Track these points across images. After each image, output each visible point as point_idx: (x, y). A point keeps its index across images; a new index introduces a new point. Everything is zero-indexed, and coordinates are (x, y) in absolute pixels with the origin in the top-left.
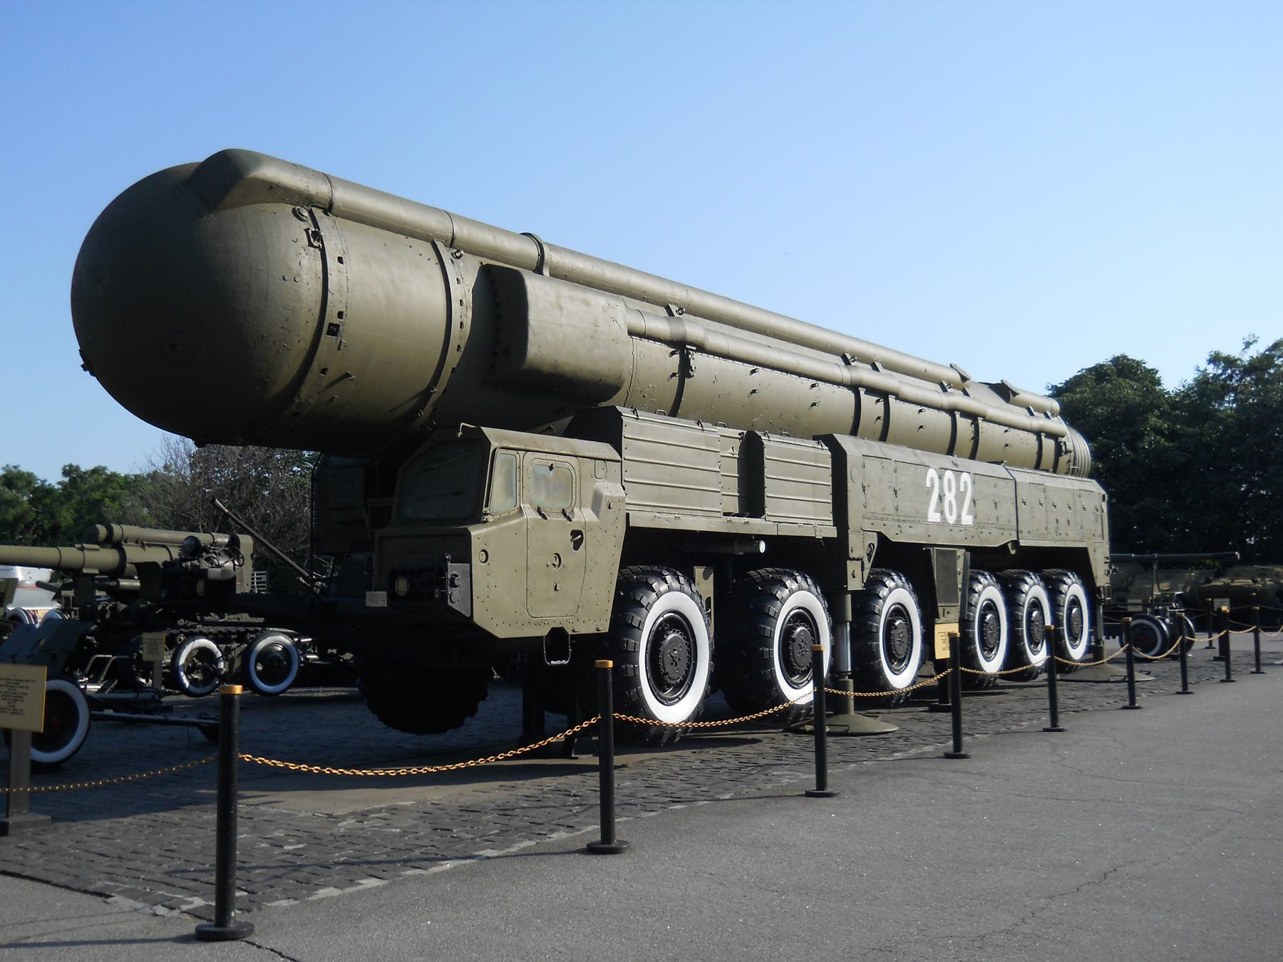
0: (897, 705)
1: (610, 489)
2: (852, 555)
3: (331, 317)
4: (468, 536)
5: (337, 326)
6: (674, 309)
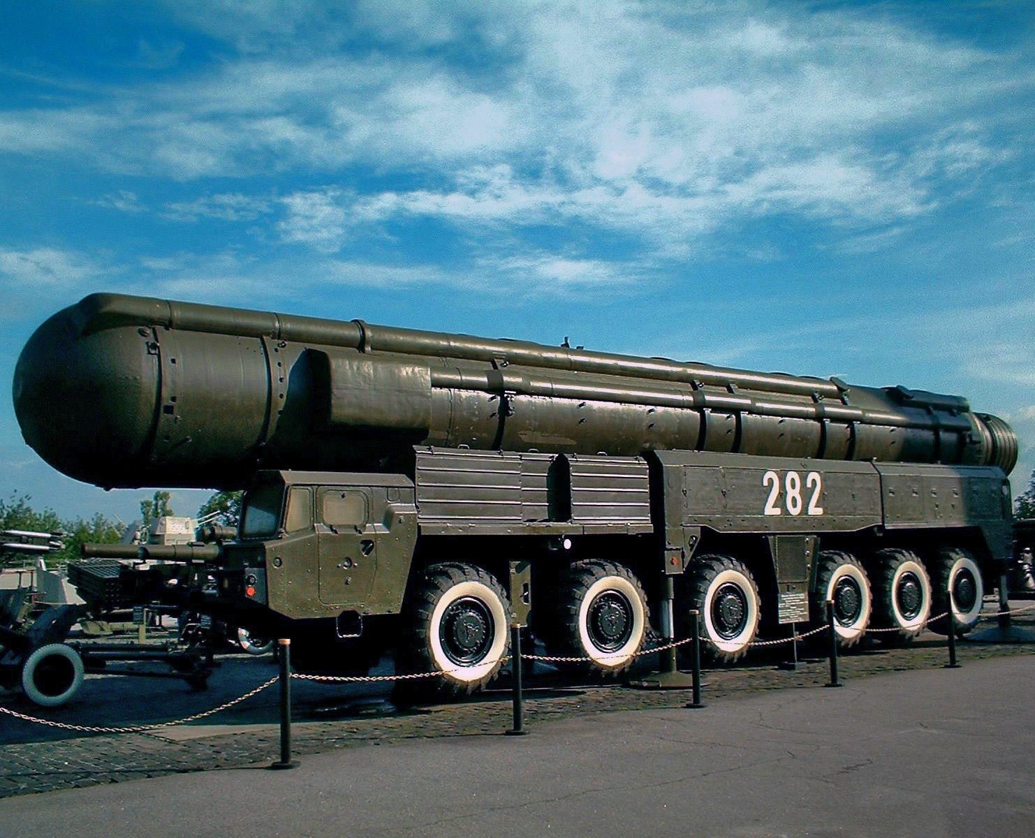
1: (402, 508)
2: (668, 547)
3: (166, 401)
4: (263, 547)
5: (172, 407)
6: (817, 395)
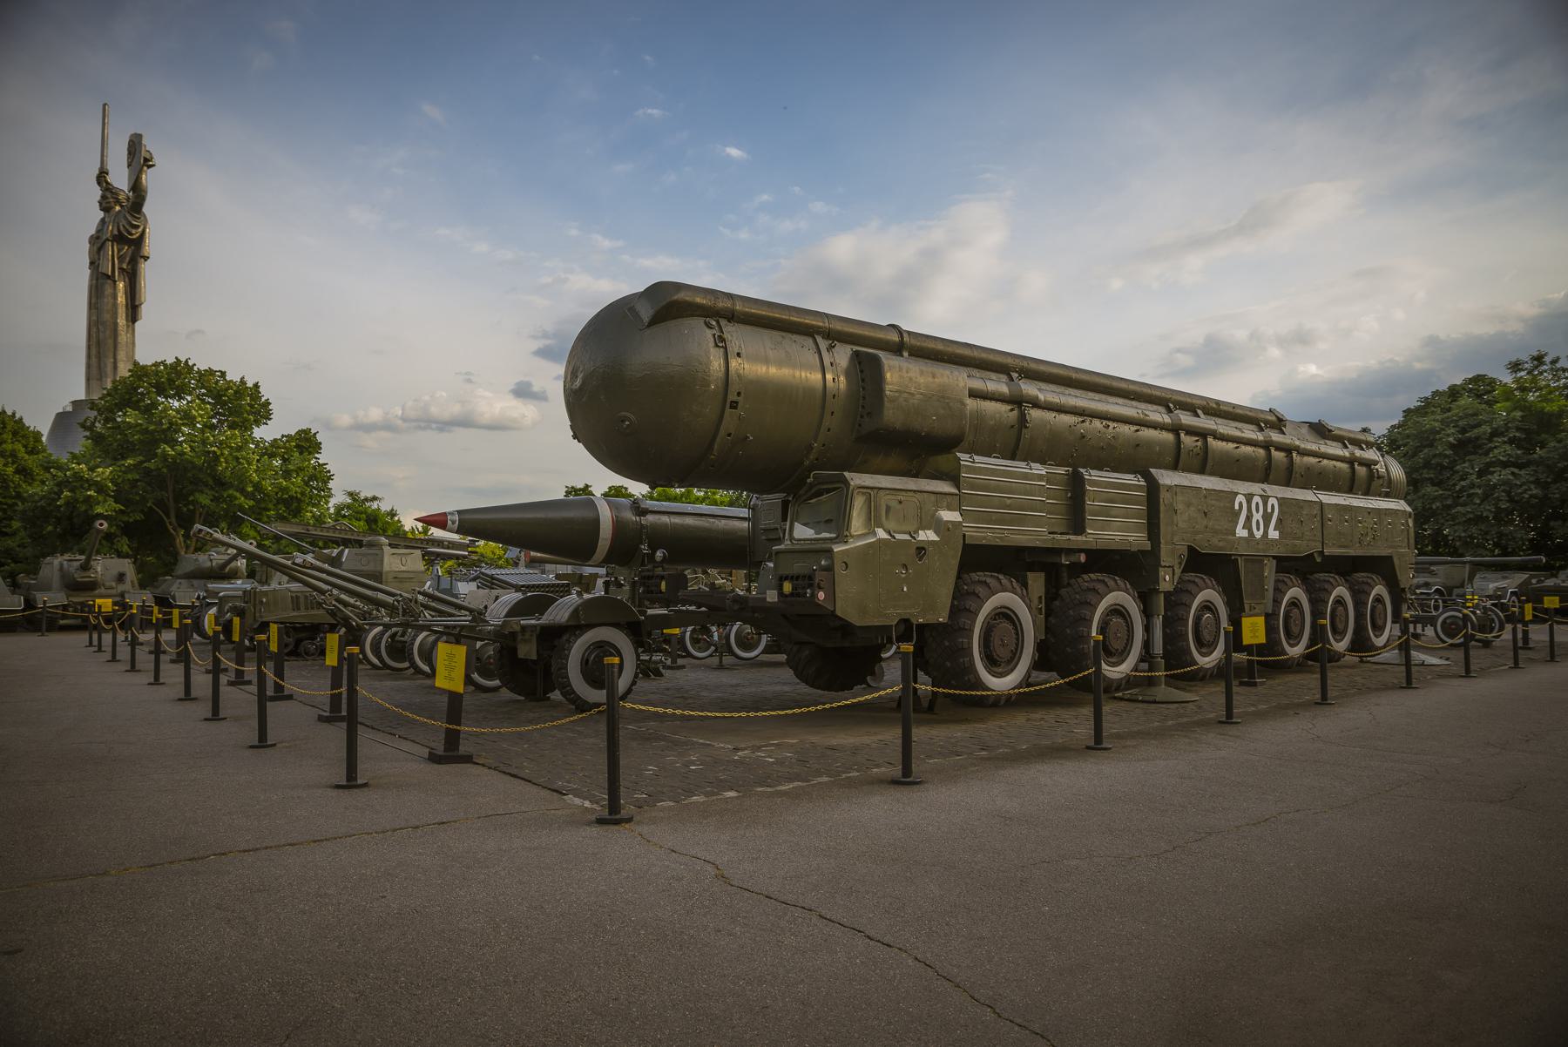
0: (1203, 679)
3: (732, 397)
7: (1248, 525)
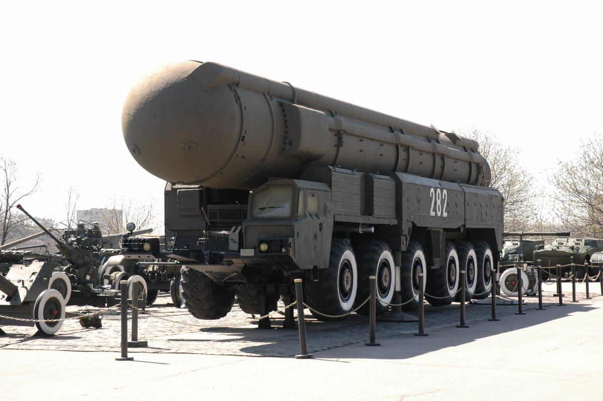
3: (243, 134)
7: (435, 210)
